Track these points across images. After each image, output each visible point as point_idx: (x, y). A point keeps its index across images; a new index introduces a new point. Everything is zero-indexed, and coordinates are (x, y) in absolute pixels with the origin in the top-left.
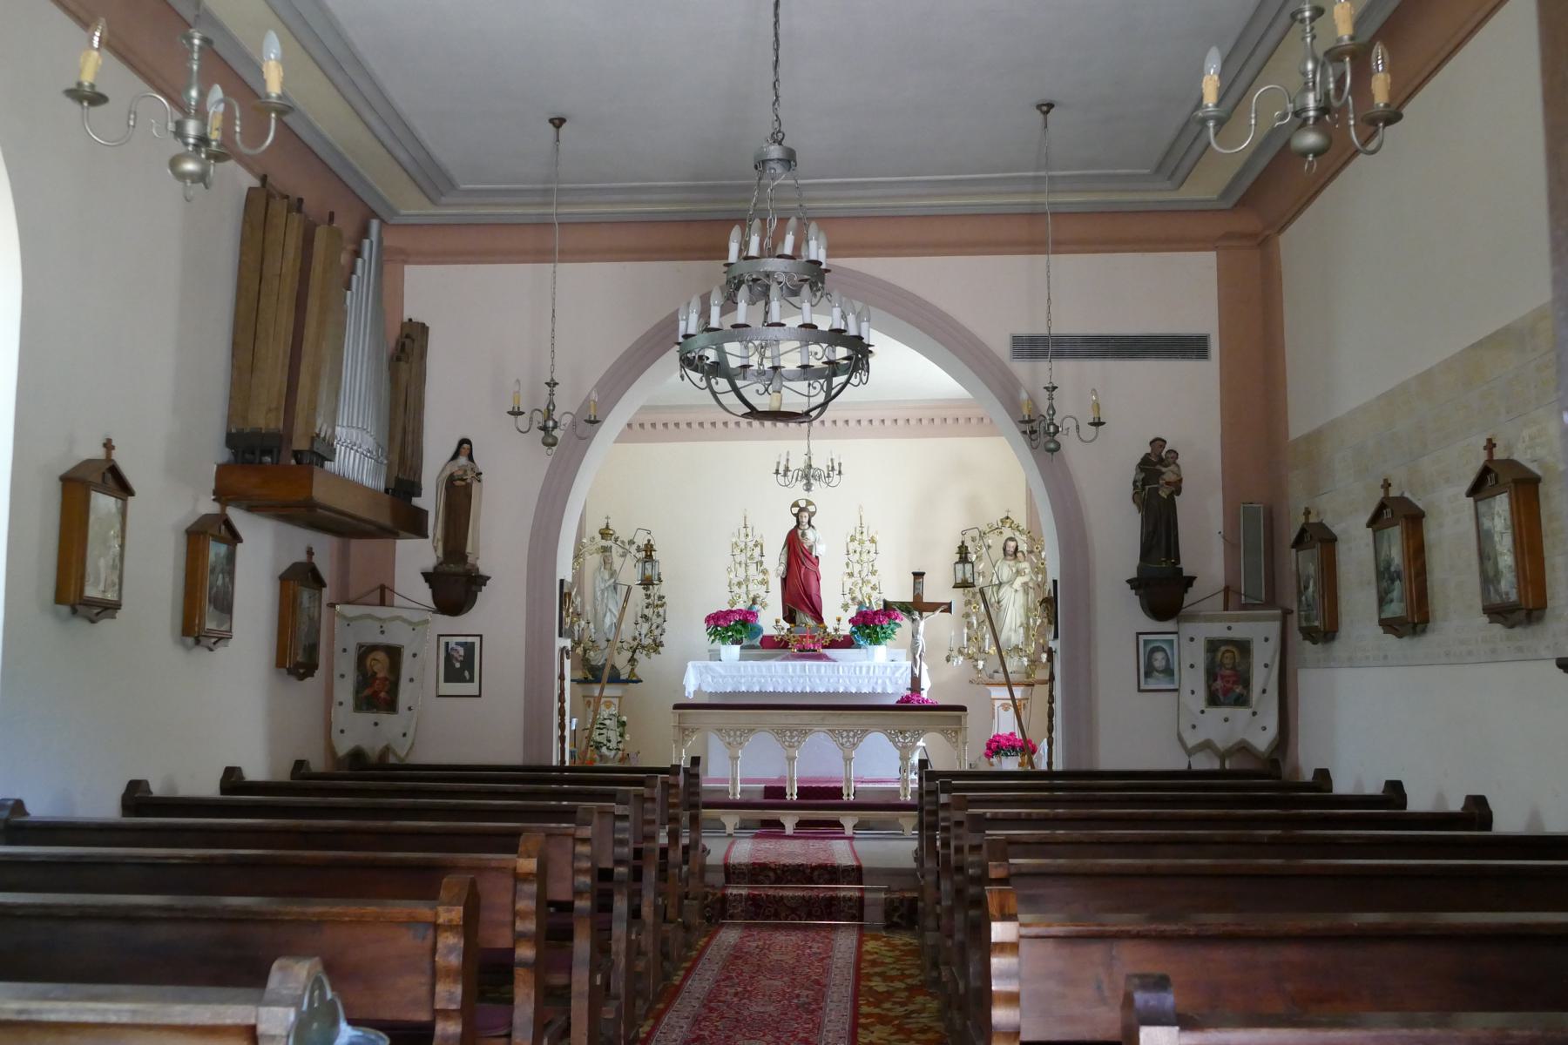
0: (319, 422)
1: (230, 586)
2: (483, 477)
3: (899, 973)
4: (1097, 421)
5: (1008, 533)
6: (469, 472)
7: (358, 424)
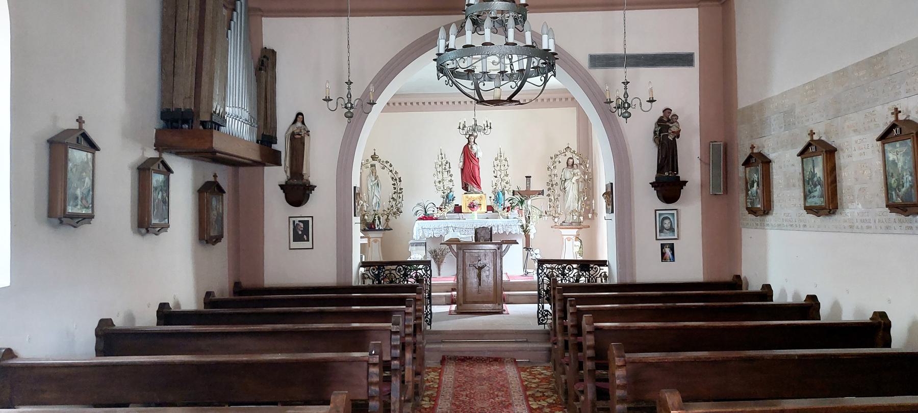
0: (215, 105)
1: (167, 198)
2: (310, 133)
3: (541, 394)
4: (651, 99)
5: (569, 155)
6: (302, 131)
7: (230, 105)
